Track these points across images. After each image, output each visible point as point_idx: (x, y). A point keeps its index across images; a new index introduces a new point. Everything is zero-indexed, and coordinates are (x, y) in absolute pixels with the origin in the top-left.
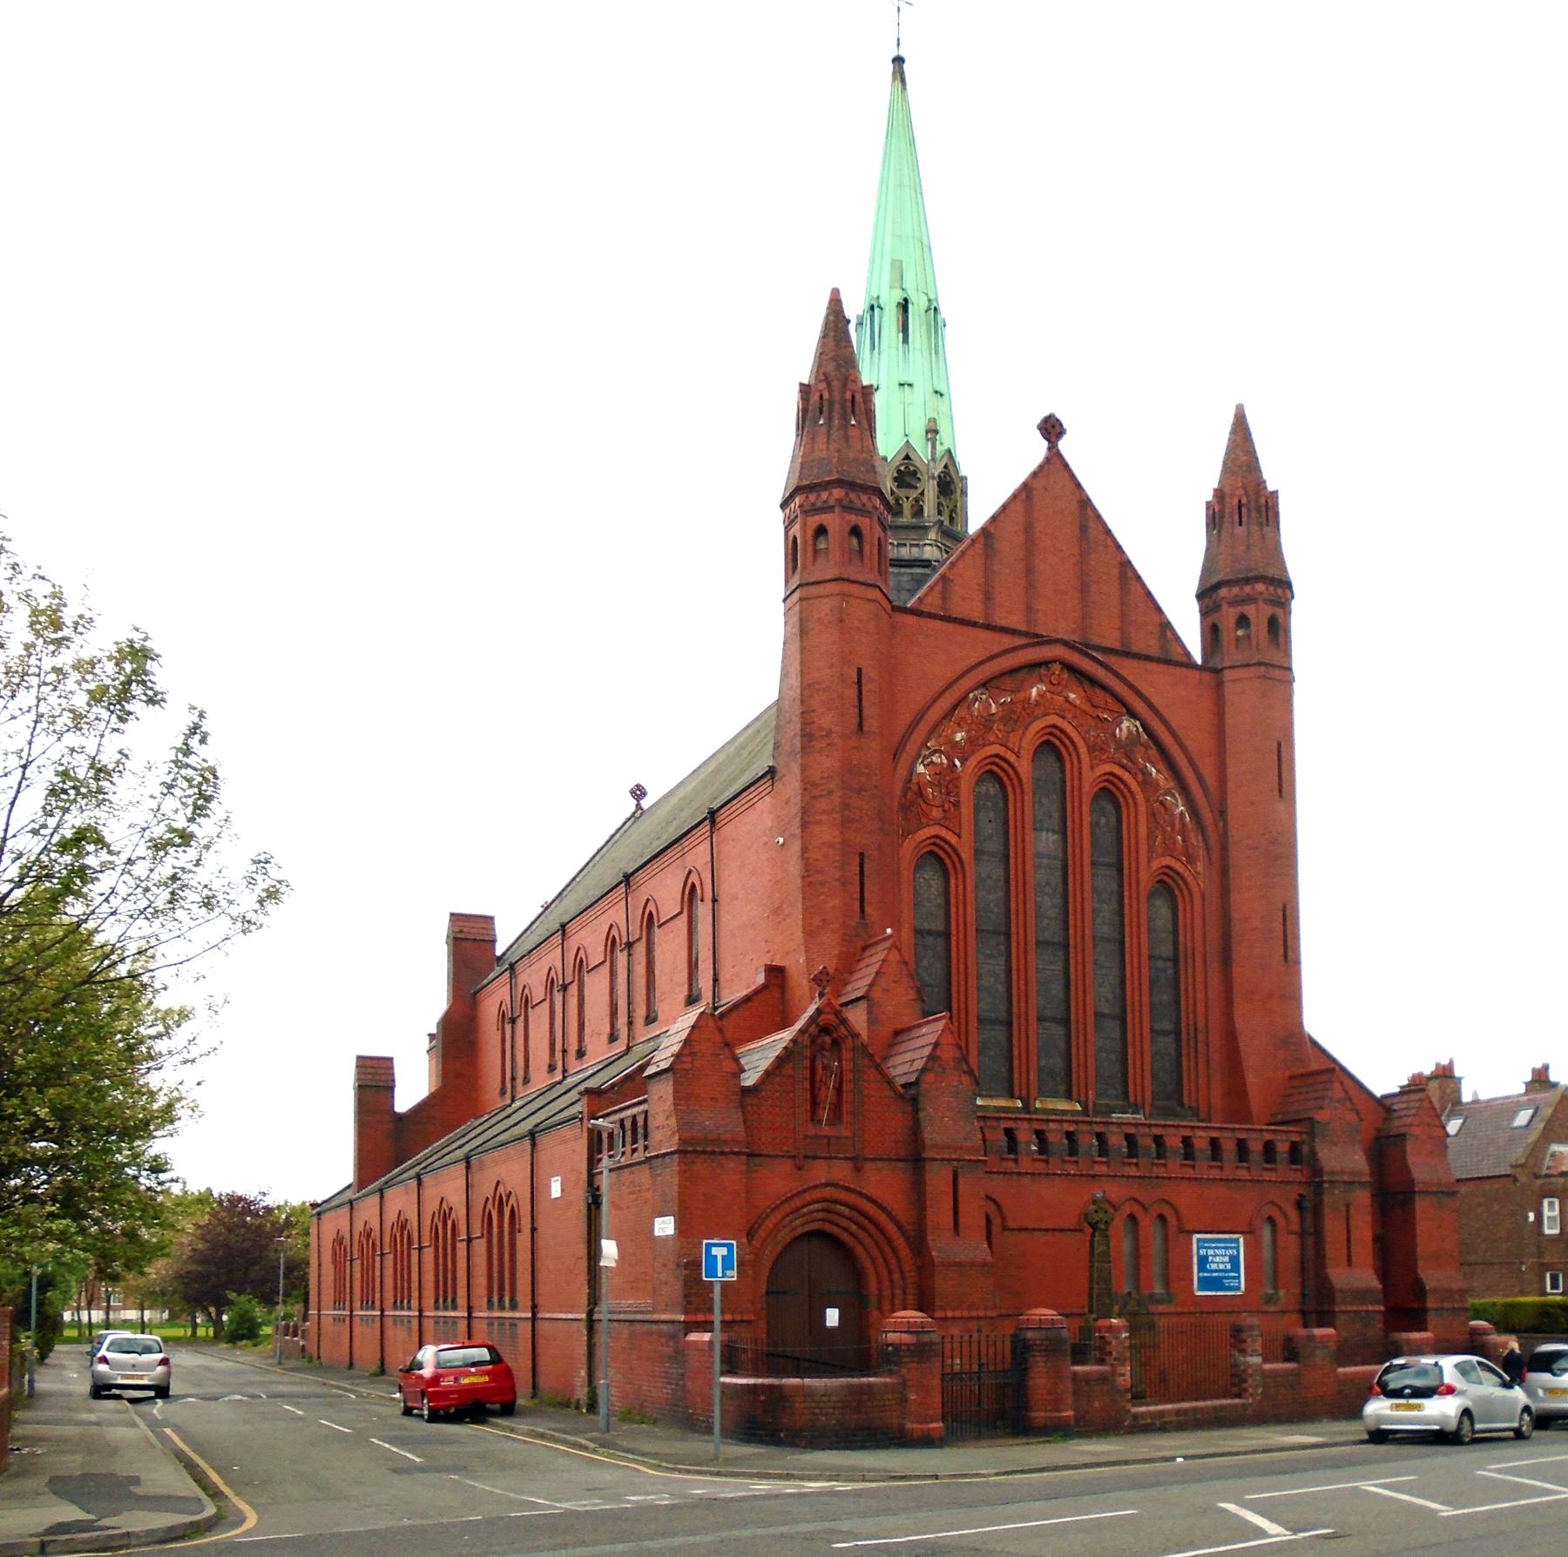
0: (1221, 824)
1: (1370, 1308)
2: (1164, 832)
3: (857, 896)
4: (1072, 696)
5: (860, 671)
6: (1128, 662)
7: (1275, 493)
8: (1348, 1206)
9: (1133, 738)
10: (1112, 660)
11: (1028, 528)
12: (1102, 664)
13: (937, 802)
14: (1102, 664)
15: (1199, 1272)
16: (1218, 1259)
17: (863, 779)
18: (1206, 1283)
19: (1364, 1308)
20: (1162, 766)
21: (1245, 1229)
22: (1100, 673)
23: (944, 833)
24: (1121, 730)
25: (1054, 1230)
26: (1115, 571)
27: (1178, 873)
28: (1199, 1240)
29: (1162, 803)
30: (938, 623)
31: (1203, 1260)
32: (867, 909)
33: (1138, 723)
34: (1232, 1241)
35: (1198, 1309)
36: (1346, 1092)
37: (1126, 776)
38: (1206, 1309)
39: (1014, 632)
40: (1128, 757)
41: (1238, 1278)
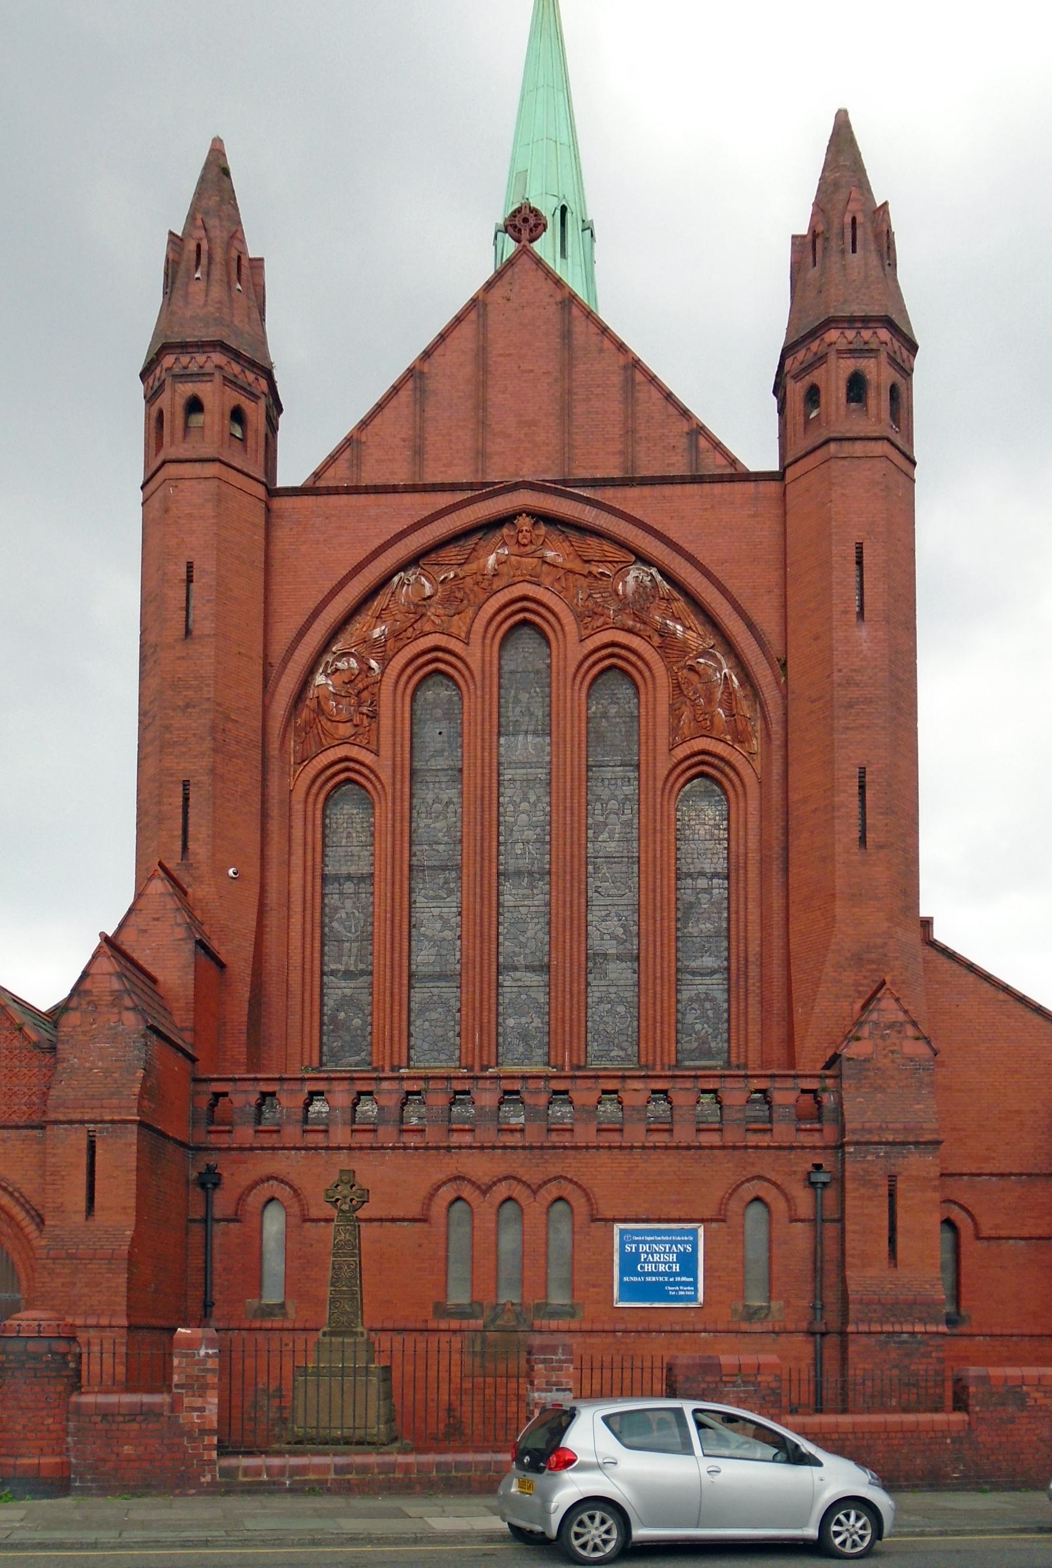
0: (783, 680)
1: (919, 1328)
2: (694, 705)
3: (179, 832)
4: (550, 554)
5: (190, 566)
6: (634, 492)
7: (885, 204)
8: (892, 1179)
9: (646, 594)
10: (607, 495)
11: (482, 352)
12: (587, 501)
13: (344, 716)
14: (587, 501)
15: (622, 1273)
16: (656, 1258)
17: (190, 693)
18: (630, 1291)
19: (907, 1328)
20: (693, 620)
21: (708, 1214)
22: (589, 515)
23: (355, 752)
24: (625, 583)
25: (381, 1220)
26: (617, 379)
27: (722, 759)
28: (623, 1232)
29: (691, 669)
30: (344, 499)
31: (630, 1262)
32: (191, 845)
33: (653, 571)
34: (682, 1232)
35: (622, 1327)
36: (906, 1012)
37: (635, 642)
38: (631, 1326)
39: (453, 487)
40: (636, 616)
41: (694, 1284)
